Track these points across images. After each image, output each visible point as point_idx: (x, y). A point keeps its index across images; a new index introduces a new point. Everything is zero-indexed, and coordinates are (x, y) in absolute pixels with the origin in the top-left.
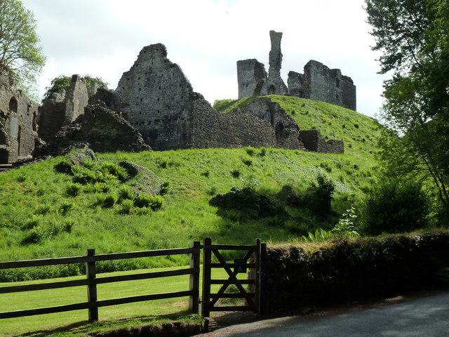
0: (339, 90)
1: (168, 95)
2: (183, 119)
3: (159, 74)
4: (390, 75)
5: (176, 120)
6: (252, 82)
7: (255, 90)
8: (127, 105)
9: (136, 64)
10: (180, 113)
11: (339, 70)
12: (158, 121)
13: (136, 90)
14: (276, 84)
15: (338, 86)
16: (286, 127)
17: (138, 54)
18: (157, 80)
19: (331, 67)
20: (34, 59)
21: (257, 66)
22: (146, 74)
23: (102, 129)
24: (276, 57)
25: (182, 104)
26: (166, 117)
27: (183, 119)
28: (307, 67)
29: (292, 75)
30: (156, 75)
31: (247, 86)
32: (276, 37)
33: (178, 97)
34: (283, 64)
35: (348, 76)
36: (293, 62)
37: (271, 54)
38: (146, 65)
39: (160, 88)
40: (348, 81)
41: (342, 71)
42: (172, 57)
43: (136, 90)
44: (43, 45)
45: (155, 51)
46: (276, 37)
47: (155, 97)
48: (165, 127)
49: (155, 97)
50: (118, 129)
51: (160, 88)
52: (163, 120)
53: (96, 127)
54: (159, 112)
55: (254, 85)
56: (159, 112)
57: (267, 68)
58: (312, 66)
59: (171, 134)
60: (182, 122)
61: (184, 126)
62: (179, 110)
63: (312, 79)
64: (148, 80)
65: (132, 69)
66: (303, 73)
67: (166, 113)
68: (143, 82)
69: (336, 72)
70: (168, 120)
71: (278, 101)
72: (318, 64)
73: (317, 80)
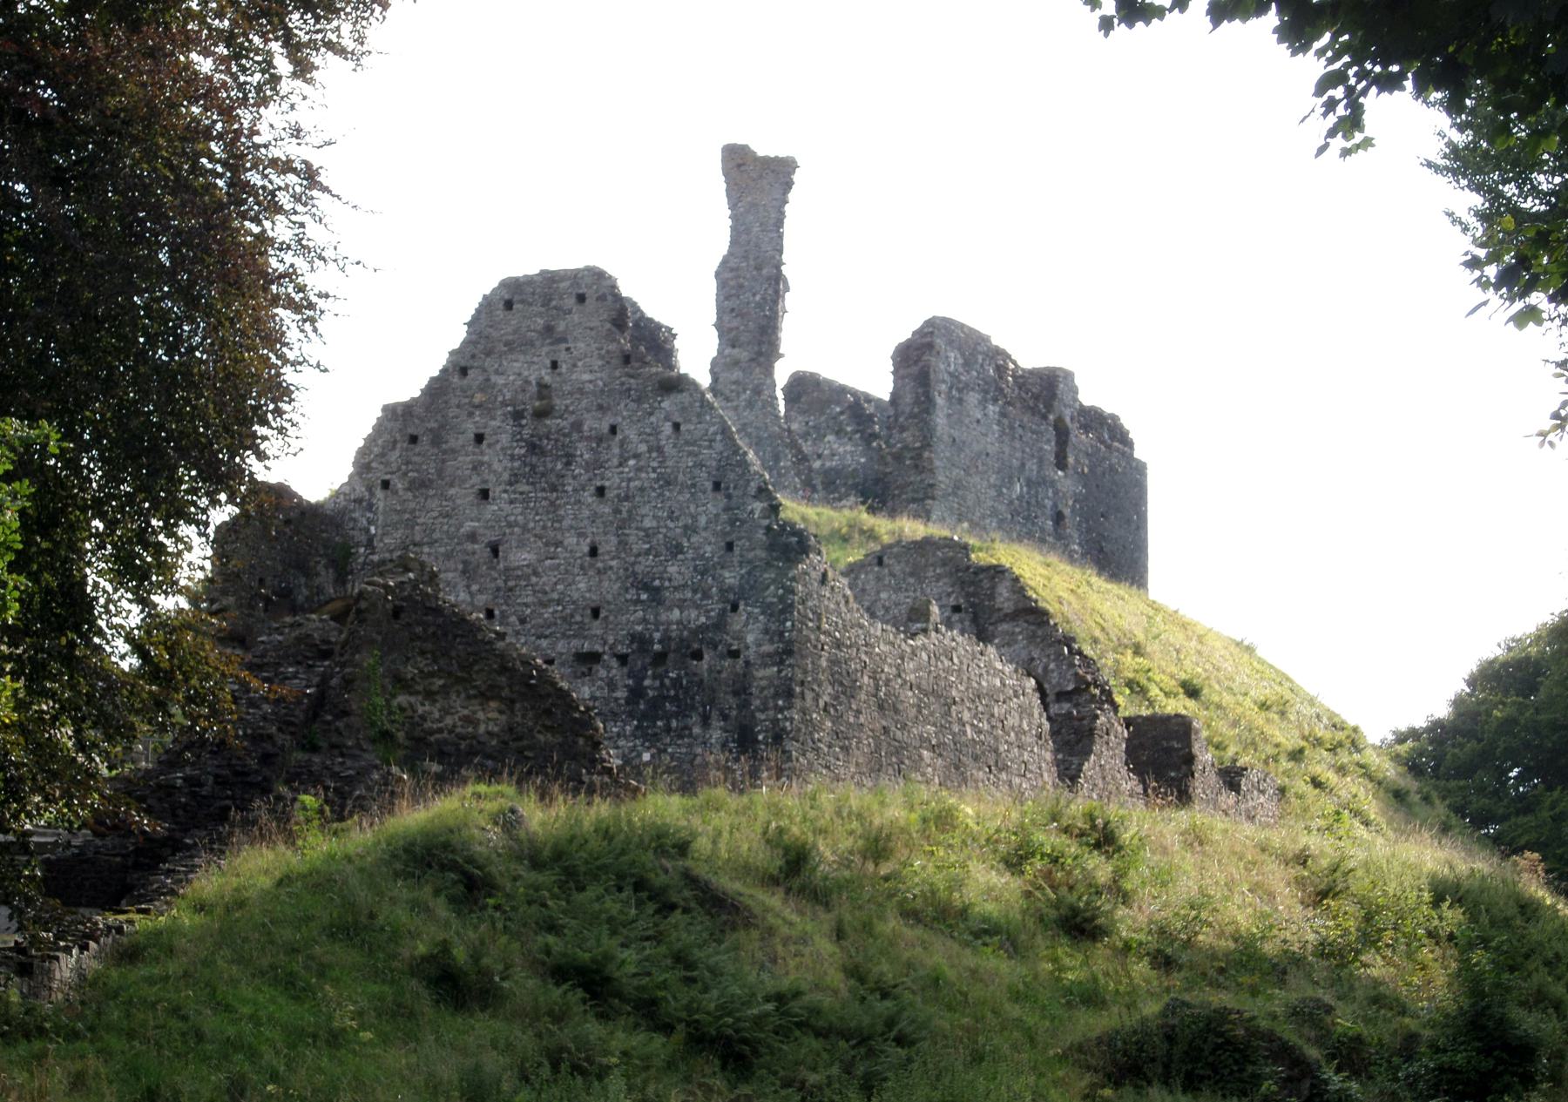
1: (648, 535)
3: (595, 424)
5: (698, 656)
9: (460, 366)
10: (720, 625)
11: (1068, 376)
12: (594, 657)
13: (463, 496)
15: (1061, 463)
18: (583, 452)
22: (518, 416)
23: (430, 695)
24: (752, 293)
25: (730, 578)
26: (634, 637)
27: (735, 654)
28: (915, 357)
30: (577, 426)
32: (757, 183)
35: (1108, 408)
36: (841, 338)
38: (521, 372)
39: (601, 491)
40: (1107, 431)
46: (757, 183)
48: (636, 693)
49: (571, 540)
51: (601, 491)
52: (623, 659)
54: (596, 613)
57: (696, 355)
61: (741, 689)
63: (940, 420)
64: (533, 448)
65: (437, 389)
67: (634, 620)
68: (497, 462)
69: (1045, 391)
72: (977, 351)
73: (967, 430)
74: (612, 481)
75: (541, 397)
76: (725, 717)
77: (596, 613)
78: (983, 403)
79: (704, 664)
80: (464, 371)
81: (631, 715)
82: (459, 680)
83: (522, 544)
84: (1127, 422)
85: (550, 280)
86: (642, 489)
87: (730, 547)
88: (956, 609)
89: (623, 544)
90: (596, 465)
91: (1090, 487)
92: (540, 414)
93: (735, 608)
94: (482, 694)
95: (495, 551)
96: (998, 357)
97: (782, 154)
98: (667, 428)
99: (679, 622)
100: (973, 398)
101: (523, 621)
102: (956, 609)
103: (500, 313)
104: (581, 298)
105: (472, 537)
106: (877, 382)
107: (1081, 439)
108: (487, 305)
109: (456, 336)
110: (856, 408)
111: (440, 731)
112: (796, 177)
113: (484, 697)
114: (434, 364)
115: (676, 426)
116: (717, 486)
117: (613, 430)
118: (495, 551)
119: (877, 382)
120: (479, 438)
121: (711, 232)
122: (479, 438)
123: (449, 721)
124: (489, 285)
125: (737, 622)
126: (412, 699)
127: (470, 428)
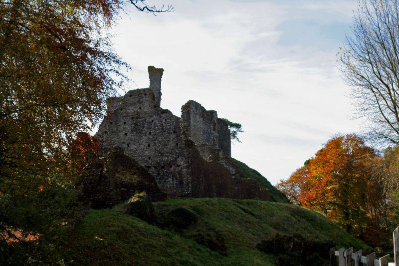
1: (160, 142)
2: (179, 166)
5: (171, 167)
10: (175, 160)
11: (215, 112)
13: (122, 135)
15: (214, 129)
18: (146, 125)
19: (208, 108)
22: (133, 118)
26: (158, 163)
30: (145, 120)
33: (172, 144)
39: (150, 133)
43: (122, 135)
45: (143, 95)
46: (155, 74)
49: (144, 143)
50: (139, 176)
52: (155, 167)
53: (118, 173)
54: (149, 158)
56: (149, 158)
61: (180, 173)
63: (192, 121)
64: (136, 125)
66: (180, 117)
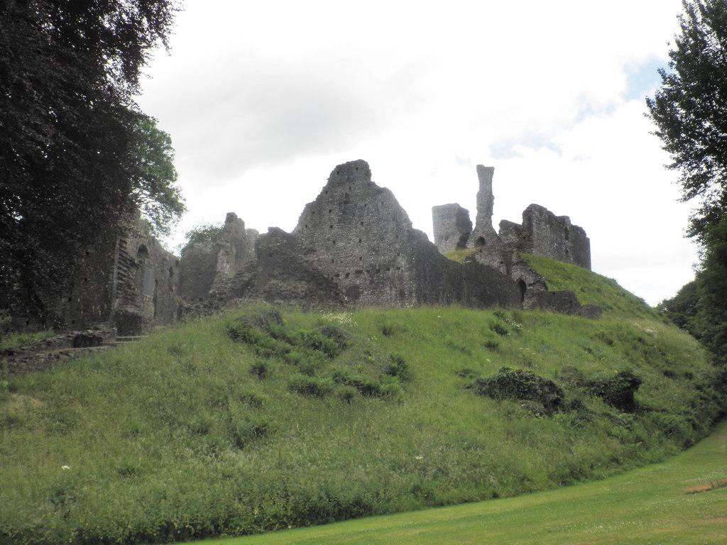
0: (569, 244)
1: (375, 235)
4: (698, 202)
5: (388, 270)
6: (453, 234)
7: (458, 244)
8: (312, 251)
10: (394, 260)
11: (568, 218)
13: (326, 228)
14: (487, 235)
15: (567, 238)
16: (530, 285)
17: (329, 177)
20: (173, 204)
21: (461, 215)
22: (340, 204)
23: (283, 280)
26: (371, 265)
27: (399, 268)
29: (505, 225)
30: (356, 205)
31: (447, 239)
32: (485, 174)
34: (495, 209)
35: (579, 226)
36: (508, 210)
37: (480, 196)
38: (340, 191)
39: (362, 223)
41: (571, 219)
42: (378, 179)
44: (184, 184)
46: (485, 174)
47: (354, 238)
48: (372, 282)
49: (354, 238)
50: (308, 282)
51: (362, 223)
52: (368, 272)
54: (361, 258)
55: (457, 239)
57: (473, 216)
58: (534, 214)
59: (380, 292)
60: (397, 273)
62: (393, 255)
64: (344, 212)
65: (320, 198)
67: (372, 260)
69: (563, 221)
70: (374, 271)
71: (4, 447)
73: (542, 231)
74: (365, 220)
75: (346, 197)
76: (396, 287)
77: (361, 258)
78: (545, 225)
79: (390, 272)
80: (327, 192)
81: (371, 288)
82: (293, 275)
83: (341, 240)
84: (589, 234)
85: (349, 164)
86: (373, 222)
87: (397, 237)
88: (502, 263)
89: (368, 239)
90: (361, 216)
91: (572, 241)
92: (346, 203)
93: (399, 255)
94: (300, 279)
95: (334, 242)
96: (550, 215)
97: (491, 166)
98: (380, 204)
99: (383, 260)
100: (543, 223)
101: (341, 262)
102: (502, 263)
103: (336, 175)
104: (357, 169)
105: (328, 239)
106: (519, 220)
107: (571, 234)
108: (333, 174)
109: (325, 183)
110: (516, 227)
111: (287, 291)
112: (494, 172)
113: (300, 280)
114: (318, 191)
115: (382, 203)
116: (394, 219)
117: (366, 205)
118: (334, 242)
119: (519, 220)
120: (330, 211)
121: (474, 185)
122: (330, 211)
123: (289, 288)
124: (333, 168)
125: (400, 259)
126: (277, 281)
127: (328, 208)
